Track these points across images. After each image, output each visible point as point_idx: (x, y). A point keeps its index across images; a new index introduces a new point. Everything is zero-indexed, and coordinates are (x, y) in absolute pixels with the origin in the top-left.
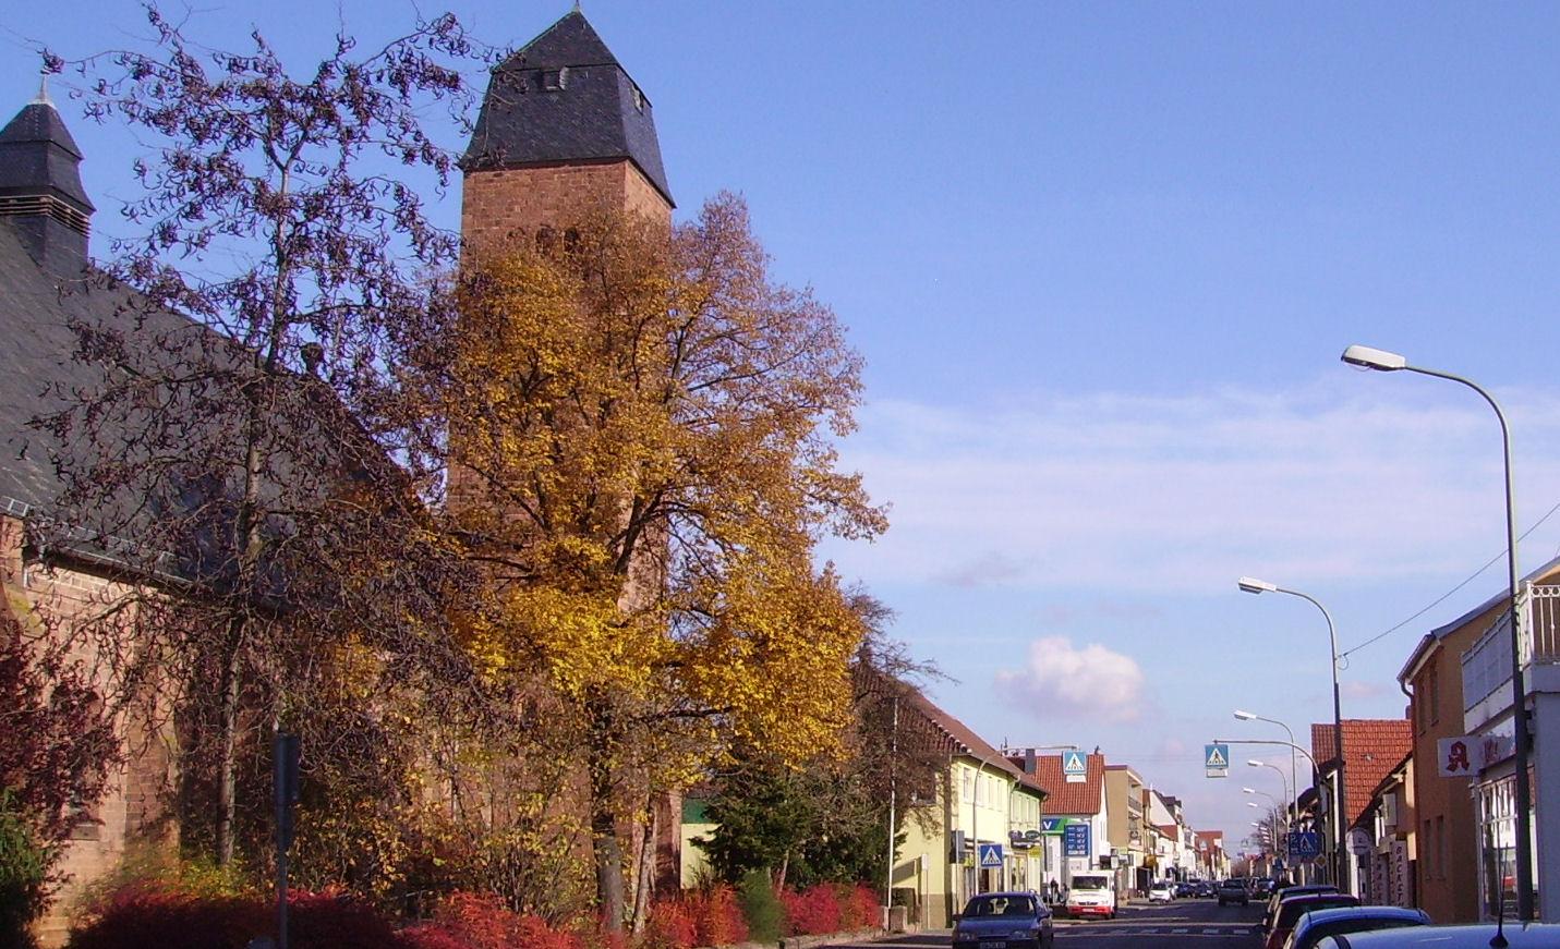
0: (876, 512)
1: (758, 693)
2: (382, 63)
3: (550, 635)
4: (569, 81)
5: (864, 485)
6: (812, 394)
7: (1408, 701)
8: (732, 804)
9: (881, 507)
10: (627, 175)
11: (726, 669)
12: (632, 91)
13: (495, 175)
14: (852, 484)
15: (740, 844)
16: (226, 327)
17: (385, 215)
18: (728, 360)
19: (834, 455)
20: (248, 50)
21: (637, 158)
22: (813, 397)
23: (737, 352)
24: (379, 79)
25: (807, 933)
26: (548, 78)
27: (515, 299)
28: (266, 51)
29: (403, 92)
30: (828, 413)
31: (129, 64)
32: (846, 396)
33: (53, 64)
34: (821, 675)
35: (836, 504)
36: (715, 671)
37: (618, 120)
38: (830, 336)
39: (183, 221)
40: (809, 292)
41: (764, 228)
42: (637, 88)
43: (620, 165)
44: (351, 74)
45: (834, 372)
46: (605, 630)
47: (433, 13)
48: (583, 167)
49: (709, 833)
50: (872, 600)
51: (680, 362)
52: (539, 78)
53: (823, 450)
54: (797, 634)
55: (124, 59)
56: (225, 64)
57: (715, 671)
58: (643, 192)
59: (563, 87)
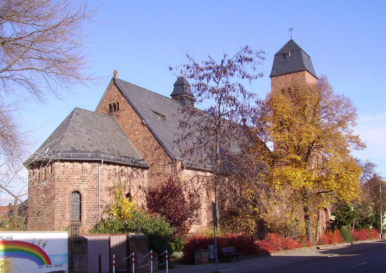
1: (337, 186)
2: (235, 58)
3: (289, 177)
5: (360, 137)
6: (346, 118)
7: (31, 243)
8: (338, 212)
9: (364, 142)
10: (306, 73)
11: (329, 182)
12: (305, 55)
13: (277, 78)
14: (357, 137)
15: (340, 221)
16: (208, 118)
17: (238, 90)
18: (327, 112)
19: (352, 131)
20: (208, 60)
21: (308, 69)
23: (329, 110)
24: (236, 61)
25: (359, 240)
27: (276, 104)
28: (212, 59)
29: (242, 63)
30: (350, 122)
31: (185, 66)
32: (354, 117)
33: (171, 69)
35: (354, 143)
37: (302, 61)
38: (350, 104)
39: (198, 97)
41: (331, 81)
42: (306, 54)
43: (304, 72)
44: (229, 61)
45: (351, 112)
46: (302, 175)
47: (244, 46)
48: (296, 73)
49: (334, 218)
50: (372, 163)
51: (315, 114)
52: (284, 55)
53: (350, 130)
54: (345, 173)
55: (184, 65)
56: (205, 63)
57: (327, 182)
58: (310, 77)
59: (290, 56)
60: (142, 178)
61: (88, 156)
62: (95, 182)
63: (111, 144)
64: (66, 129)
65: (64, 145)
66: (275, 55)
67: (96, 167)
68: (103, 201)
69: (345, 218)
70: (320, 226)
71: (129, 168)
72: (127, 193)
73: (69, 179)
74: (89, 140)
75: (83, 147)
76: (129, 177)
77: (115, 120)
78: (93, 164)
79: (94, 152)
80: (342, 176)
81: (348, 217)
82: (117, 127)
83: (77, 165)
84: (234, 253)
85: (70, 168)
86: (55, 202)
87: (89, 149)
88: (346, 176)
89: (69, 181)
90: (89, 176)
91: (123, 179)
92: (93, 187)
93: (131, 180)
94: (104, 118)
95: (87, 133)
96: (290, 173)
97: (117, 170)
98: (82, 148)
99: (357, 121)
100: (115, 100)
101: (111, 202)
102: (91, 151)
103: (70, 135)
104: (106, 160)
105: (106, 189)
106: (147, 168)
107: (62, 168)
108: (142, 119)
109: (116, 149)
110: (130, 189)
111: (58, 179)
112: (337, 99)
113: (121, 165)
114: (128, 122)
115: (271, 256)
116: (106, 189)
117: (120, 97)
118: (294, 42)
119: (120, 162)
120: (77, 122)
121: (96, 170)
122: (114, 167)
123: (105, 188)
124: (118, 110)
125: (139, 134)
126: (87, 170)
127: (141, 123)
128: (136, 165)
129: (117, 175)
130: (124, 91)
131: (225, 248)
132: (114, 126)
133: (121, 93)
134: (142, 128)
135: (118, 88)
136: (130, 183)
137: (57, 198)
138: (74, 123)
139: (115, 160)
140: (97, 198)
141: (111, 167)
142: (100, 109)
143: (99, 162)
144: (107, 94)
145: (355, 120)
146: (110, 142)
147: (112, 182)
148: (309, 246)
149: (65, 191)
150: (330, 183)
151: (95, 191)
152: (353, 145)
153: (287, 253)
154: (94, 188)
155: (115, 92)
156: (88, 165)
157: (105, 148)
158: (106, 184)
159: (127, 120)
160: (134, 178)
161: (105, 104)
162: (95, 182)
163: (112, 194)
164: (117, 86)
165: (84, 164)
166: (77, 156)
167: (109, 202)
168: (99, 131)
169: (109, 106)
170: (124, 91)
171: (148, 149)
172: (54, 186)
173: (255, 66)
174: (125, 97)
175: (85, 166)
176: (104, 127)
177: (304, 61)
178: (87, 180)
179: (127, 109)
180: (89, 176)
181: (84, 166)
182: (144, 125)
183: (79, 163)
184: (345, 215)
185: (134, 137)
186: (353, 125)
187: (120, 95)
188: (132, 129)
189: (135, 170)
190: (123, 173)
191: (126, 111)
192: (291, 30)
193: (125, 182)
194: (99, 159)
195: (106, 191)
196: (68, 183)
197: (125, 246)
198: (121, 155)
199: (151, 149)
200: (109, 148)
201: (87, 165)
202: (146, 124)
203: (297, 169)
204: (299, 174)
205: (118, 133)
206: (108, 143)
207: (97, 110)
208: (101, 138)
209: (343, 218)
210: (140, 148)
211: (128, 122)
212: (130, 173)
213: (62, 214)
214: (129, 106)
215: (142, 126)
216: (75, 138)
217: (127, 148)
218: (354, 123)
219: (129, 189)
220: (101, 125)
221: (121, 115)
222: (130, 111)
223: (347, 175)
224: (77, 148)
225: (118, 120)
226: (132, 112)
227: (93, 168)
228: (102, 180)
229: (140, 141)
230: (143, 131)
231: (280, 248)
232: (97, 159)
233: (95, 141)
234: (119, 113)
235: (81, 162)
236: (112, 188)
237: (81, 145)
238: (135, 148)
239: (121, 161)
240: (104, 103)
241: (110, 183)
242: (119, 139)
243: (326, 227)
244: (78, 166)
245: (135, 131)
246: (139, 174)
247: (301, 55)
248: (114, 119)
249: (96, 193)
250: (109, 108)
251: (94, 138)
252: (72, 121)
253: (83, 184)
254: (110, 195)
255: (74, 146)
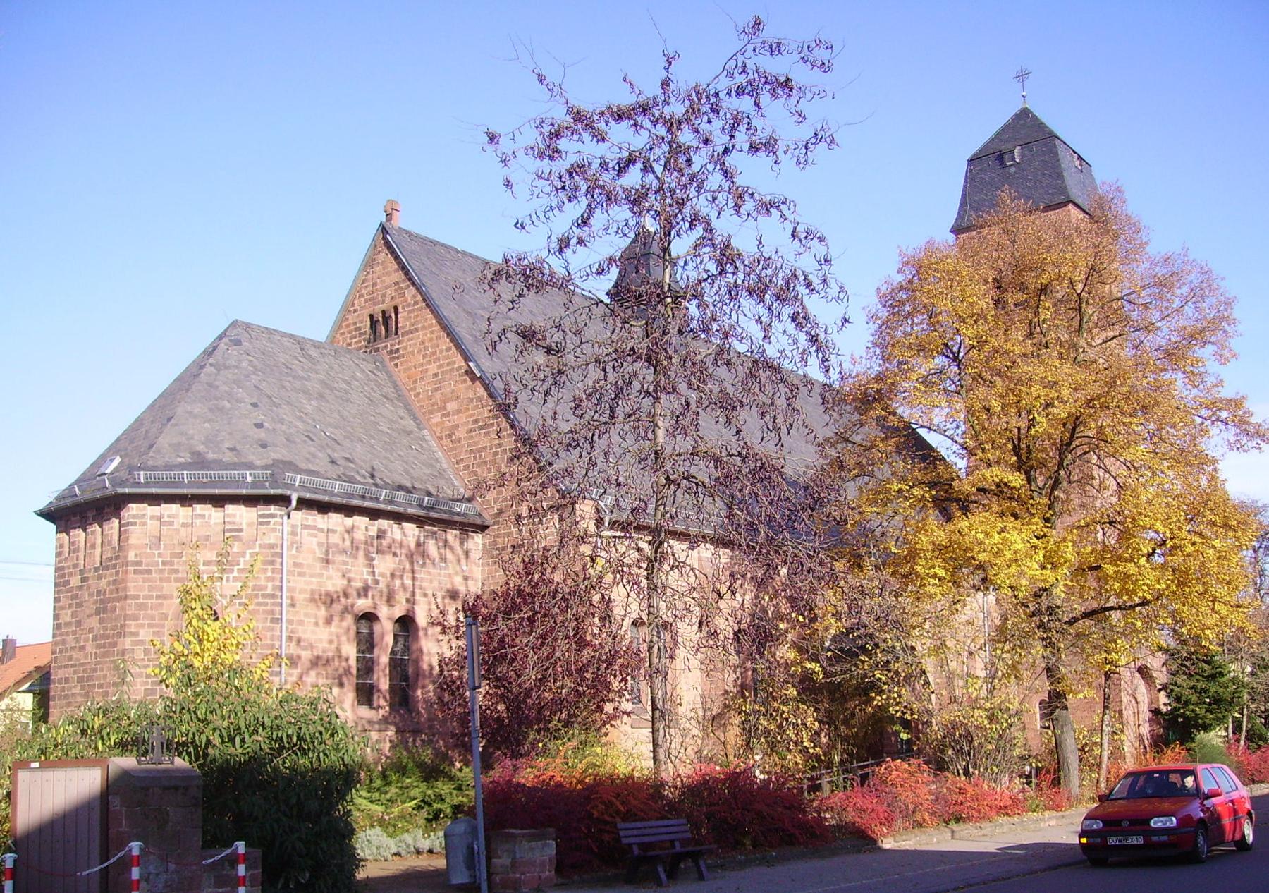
0: (1260, 425)
1: (1159, 584)
4: (1022, 156)
8: (1179, 681)
14: (1235, 404)
21: (1079, 201)
22: (1196, 336)
25: (1262, 782)
26: (1006, 157)
33: (492, 138)
34: (1214, 564)
36: (1120, 568)
37: (1060, 175)
40: (1186, 251)
42: (1075, 152)
43: (1066, 208)
47: (746, 19)
52: (1000, 158)
60: (463, 562)
61: (245, 482)
62: (269, 574)
63: (346, 443)
64: (187, 390)
65: (167, 445)
66: (971, 161)
67: (273, 520)
68: (299, 641)
69: (1204, 703)
70: (1126, 732)
71: (411, 528)
72: (399, 612)
73: (178, 563)
74: (259, 426)
75: (232, 449)
76: (410, 557)
77: (384, 367)
78: (262, 509)
79: (266, 467)
80: (1178, 542)
81: (1217, 701)
82: (389, 390)
83: (207, 513)
84: (684, 842)
85: (184, 525)
86: (127, 643)
87: (251, 458)
88: (1194, 544)
89: (177, 571)
90: (248, 552)
91: (385, 565)
92: (261, 590)
93: (416, 568)
94: (342, 359)
95: (255, 405)
96: (981, 536)
97: (360, 532)
98: (229, 454)
99: (1235, 344)
100: (387, 300)
101: (334, 646)
102: (258, 463)
103: (196, 411)
104: (308, 496)
105: (313, 600)
106: (483, 528)
107: (152, 525)
108: (467, 359)
109: (364, 461)
110: (411, 601)
111: (139, 563)
112: (1160, 271)
113: (374, 514)
114: (427, 371)
115: (880, 848)
116: (313, 600)
117: (401, 289)
118: (1034, 116)
119: (366, 504)
120: (227, 368)
121: (274, 530)
122: (349, 521)
123: (308, 596)
124: (396, 334)
125: (459, 412)
126: (241, 530)
127: (466, 372)
128: (435, 515)
129: (357, 549)
130: (414, 266)
131: (638, 824)
132: (379, 385)
133: (407, 273)
134: (467, 389)
135: (397, 258)
136: (414, 579)
137: (133, 630)
138: (219, 370)
139: (351, 496)
140: (273, 629)
141: (335, 519)
142: (342, 334)
143: (283, 500)
144: (364, 281)
145: (1230, 340)
146: (346, 437)
147: (340, 574)
148: (1058, 806)
149: (161, 605)
150: (1131, 572)
151: (266, 604)
152: (1225, 434)
153: (957, 835)
154: (263, 596)
155: (388, 274)
156: (245, 514)
157: (320, 455)
158: (313, 579)
159: (422, 365)
160: (428, 561)
161: (358, 316)
162: (269, 574)
163: (336, 619)
164: (393, 252)
165: (230, 508)
166: (205, 480)
167: (326, 645)
168: (310, 400)
169: (369, 323)
170: (415, 268)
171: (486, 462)
172: (125, 589)
173: (803, 106)
174: (417, 289)
175: (234, 516)
176: (332, 389)
177: (1065, 174)
178: (241, 567)
179: (424, 328)
180: (248, 552)
181: (229, 515)
182: (474, 378)
183: (214, 506)
184: (1205, 692)
185: (443, 422)
186: (1223, 360)
187: (404, 281)
188: (438, 395)
189: (435, 533)
190: (385, 543)
191: (421, 333)
192: (1023, 76)
193: (393, 575)
194: (279, 491)
195: (312, 605)
196: (173, 576)
197: (96, 815)
198: (379, 482)
199: (494, 462)
200: (336, 455)
201: (241, 514)
202: (478, 375)
203: (1010, 522)
204: (1019, 538)
205: (388, 409)
206: (335, 440)
207: (332, 339)
208: (310, 421)
209: (1197, 704)
210: (462, 460)
211: (427, 371)
212: (413, 545)
213: (149, 687)
214: (430, 316)
215: (469, 383)
216: (209, 421)
217: (411, 459)
218: (1225, 352)
219: (408, 601)
220: (323, 382)
221: (405, 348)
222: (432, 332)
223: (1197, 539)
224: (211, 456)
225: (396, 365)
226: (438, 338)
227: (261, 523)
228: (296, 565)
229: (461, 433)
230: (471, 400)
231: (926, 816)
232: (272, 492)
233: (284, 432)
234: (399, 343)
235: (219, 501)
236: (338, 597)
237: (227, 445)
238: (443, 460)
239: (377, 500)
240: (355, 311)
241: (329, 578)
242: (385, 429)
243: (1152, 736)
244: (210, 515)
245: (445, 401)
246: (452, 549)
247: (1056, 154)
248: (381, 363)
249: (272, 612)
250: (368, 330)
251: (282, 421)
252: (211, 365)
253: (225, 579)
254: (329, 621)
255: (201, 448)
